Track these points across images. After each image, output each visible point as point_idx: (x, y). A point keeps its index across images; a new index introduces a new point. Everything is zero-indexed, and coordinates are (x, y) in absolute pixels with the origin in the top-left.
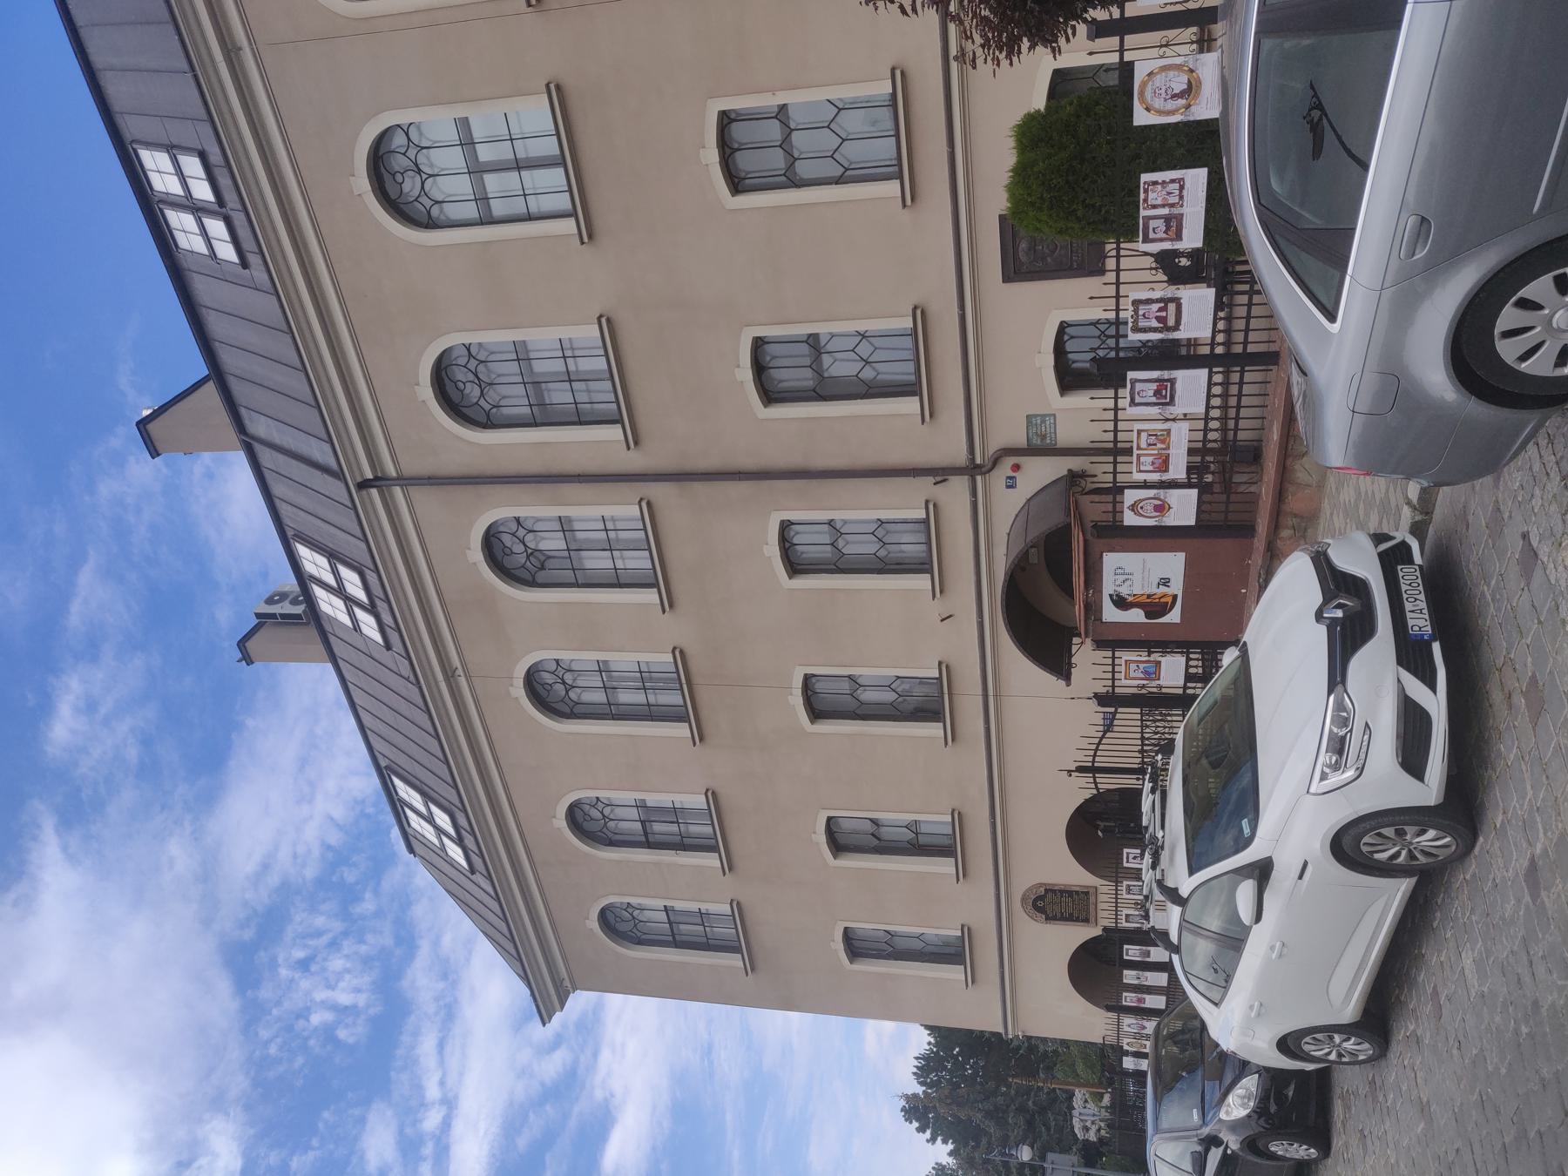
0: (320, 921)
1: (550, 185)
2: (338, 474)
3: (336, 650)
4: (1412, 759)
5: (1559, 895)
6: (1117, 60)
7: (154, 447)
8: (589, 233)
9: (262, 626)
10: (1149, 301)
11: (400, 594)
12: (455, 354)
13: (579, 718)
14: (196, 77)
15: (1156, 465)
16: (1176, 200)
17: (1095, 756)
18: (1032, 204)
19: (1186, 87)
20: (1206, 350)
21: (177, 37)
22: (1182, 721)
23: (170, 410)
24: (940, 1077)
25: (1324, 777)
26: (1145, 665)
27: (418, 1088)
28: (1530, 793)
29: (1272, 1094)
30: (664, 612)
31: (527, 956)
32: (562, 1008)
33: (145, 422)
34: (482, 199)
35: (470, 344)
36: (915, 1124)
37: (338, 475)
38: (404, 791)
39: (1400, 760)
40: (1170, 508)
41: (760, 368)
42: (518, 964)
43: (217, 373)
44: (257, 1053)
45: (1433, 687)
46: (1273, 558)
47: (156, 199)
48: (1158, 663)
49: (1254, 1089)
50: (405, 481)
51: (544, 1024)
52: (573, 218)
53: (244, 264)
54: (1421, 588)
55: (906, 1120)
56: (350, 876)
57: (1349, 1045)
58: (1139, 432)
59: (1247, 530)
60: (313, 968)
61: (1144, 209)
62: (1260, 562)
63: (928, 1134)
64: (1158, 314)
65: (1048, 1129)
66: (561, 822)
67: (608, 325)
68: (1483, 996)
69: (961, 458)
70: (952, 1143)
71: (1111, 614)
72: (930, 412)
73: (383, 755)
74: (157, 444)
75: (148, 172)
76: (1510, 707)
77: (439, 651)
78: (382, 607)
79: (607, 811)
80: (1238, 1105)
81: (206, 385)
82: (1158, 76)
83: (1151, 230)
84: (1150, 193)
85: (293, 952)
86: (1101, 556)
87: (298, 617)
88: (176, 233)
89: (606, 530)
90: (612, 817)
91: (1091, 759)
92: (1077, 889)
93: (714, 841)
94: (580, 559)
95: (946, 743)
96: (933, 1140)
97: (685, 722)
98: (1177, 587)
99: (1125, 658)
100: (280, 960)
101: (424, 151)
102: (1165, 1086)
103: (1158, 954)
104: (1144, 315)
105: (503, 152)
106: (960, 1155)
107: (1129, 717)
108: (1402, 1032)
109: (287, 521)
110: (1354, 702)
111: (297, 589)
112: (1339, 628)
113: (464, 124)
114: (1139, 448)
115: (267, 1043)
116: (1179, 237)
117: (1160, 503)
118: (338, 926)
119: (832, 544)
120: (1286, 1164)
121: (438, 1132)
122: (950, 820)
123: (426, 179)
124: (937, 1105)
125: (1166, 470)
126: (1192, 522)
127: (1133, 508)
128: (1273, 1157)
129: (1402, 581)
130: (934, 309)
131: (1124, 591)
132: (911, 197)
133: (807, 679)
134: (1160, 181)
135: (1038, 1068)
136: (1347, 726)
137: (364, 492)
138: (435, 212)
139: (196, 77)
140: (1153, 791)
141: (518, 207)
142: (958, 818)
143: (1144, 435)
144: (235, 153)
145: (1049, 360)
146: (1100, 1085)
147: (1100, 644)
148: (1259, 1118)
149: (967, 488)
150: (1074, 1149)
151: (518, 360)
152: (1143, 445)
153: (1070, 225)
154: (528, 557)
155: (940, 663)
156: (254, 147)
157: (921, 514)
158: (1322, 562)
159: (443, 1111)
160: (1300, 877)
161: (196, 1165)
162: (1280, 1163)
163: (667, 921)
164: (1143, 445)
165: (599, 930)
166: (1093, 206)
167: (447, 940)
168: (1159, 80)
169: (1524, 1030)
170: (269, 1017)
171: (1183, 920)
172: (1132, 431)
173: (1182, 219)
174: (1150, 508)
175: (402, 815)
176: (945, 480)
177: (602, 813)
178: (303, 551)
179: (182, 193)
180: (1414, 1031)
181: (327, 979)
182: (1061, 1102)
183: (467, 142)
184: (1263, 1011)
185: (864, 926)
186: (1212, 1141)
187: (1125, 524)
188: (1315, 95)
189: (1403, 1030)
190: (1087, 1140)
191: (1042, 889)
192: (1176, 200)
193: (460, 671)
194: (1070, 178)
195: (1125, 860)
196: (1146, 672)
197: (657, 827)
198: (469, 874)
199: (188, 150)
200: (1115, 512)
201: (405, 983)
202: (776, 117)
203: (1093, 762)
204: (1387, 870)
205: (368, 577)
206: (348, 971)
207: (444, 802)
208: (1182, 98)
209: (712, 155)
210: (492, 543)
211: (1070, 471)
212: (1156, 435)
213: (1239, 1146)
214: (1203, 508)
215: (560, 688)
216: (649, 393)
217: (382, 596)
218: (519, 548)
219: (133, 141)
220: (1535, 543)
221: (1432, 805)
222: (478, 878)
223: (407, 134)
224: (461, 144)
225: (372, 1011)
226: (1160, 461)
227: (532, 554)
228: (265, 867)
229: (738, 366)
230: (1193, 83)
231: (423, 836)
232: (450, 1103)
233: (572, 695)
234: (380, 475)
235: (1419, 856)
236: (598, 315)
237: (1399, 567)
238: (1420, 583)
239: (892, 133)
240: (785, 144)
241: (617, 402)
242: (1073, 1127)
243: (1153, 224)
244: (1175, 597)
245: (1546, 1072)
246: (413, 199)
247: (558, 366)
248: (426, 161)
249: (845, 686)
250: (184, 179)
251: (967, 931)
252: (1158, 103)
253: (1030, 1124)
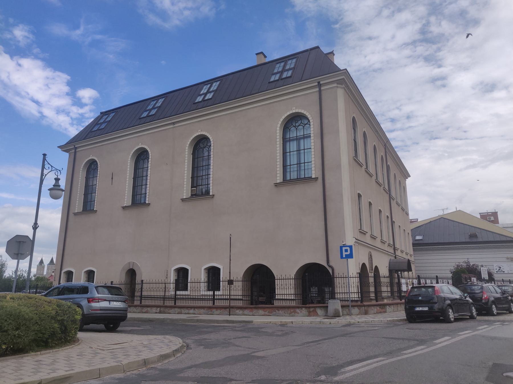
50: (320, 91)
89: (304, 149)
123: (308, 124)
203: (373, 277)
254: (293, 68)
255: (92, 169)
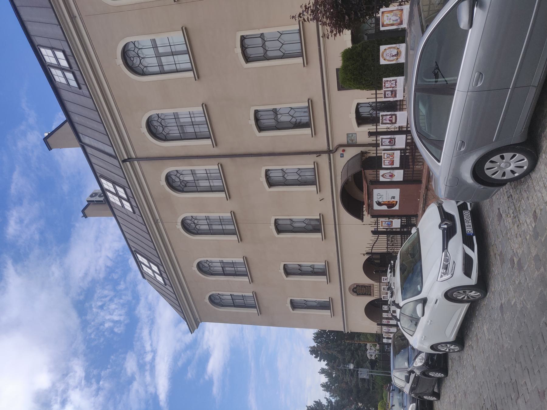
0: (106, 292)
1: (184, 60)
2: (115, 157)
3: (115, 212)
4: (467, 272)
5: (508, 317)
6: (375, 143)
7: (50, 147)
8: (198, 76)
9: (89, 205)
10: (386, 115)
11: (137, 193)
12: (153, 117)
13: (200, 234)
14: (61, 28)
15: (390, 163)
16: (394, 86)
17: (372, 249)
18: (348, 79)
19: (396, 53)
20: (405, 129)
21: (54, 14)
22: (400, 248)
23: (54, 133)
24: (322, 340)
25: (441, 276)
26: (388, 222)
27: (143, 347)
28: (501, 285)
29: (430, 358)
30: (227, 200)
31: (182, 305)
32: (197, 328)
33: (46, 138)
34: (161, 65)
35: (158, 114)
36: (314, 356)
37: (115, 157)
38: (141, 258)
39: (464, 272)
40: (394, 176)
41: (257, 120)
42: (182, 314)
43: (69, 119)
44: (87, 337)
45: (473, 250)
46: (426, 205)
47: (47, 64)
48: (392, 222)
49: (424, 357)
50: (138, 159)
51: (192, 334)
52: (192, 72)
53: (80, 88)
54: (470, 218)
55: (311, 354)
56: (115, 276)
57: (452, 347)
58: (384, 154)
59: (419, 182)
60: (105, 308)
61: (384, 88)
62: (423, 192)
63: (318, 358)
64: (389, 119)
65: (359, 356)
66: (195, 268)
67: (206, 107)
68: (489, 340)
69: (325, 148)
70: (326, 361)
71: (376, 207)
72: (315, 133)
73: (133, 246)
74: (51, 146)
75: (44, 56)
76: (495, 258)
77: (150, 211)
78: (132, 200)
79: (210, 264)
80: (419, 362)
81: (66, 123)
82: (388, 50)
83: (387, 95)
84: (386, 84)
85: (97, 303)
86: (373, 190)
87: (101, 201)
88: (45, 57)
89: (207, 173)
90: (212, 266)
91: (371, 250)
92: (367, 285)
93: (246, 273)
94: (198, 183)
95: (323, 240)
96: (320, 360)
97: (236, 235)
98: (397, 199)
99: (381, 220)
100: (93, 306)
101: (141, 50)
102: (396, 353)
103: (393, 322)
104: (385, 119)
105: (168, 49)
106: (329, 365)
107: (383, 238)
108: (468, 344)
109: (97, 171)
110: (451, 255)
111: (101, 191)
112: (446, 231)
113: (154, 41)
114: (384, 158)
115: (90, 334)
116: (395, 96)
117: (391, 174)
118: (112, 294)
119: (283, 176)
120: (434, 378)
121: (151, 362)
122: (325, 264)
124: (321, 350)
125: (393, 165)
126: (402, 180)
127: (383, 176)
128: (431, 377)
129: (464, 216)
130: (315, 100)
131: (380, 200)
132: (306, 63)
133: (276, 220)
134: (389, 80)
135: (355, 336)
136: (448, 262)
137: (124, 163)
138: (145, 69)
139: (61, 28)
140: (391, 272)
141: (173, 67)
142: (327, 263)
143: (386, 155)
144: (75, 51)
145: (354, 115)
146: (376, 341)
147: (373, 216)
148: (426, 366)
149: (327, 158)
150: (367, 362)
151: (175, 118)
152: (386, 157)
153: (360, 86)
154: (181, 183)
155: (320, 214)
156: (83, 53)
157: (313, 167)
158: (441, 208)
159: (152, 354)
160: (436, 303)
161: (69, 375)
162: (433, 378)
163: (231, 299)
164: (386, 157)
165: (209, 302)
166: (368, 80)
167: (150, 297)
168: (388, 51)
169: (500, 352)
170: (90, 325)
171: (401, 313)
172: (382, 153)
173: (396, 91)
174: (388, 176)
175: (140, 266)
176: (320, 155)
177: (209, 265)
178: (103, 181)
179: (57, 63)
180: (471, 344)
181: (109, 312)
182: (363, 347)
183: (155, 46)
184: (426, 338)
185: (297, 299)
186: (412, 372)
187: (380, 181)
188: (437, 65)
189: (468, 343)
190: (372, 359)
191: (356, 285)
192: (394, 86)
193: (159, 221)
194: (360, 71)
195: (382, 280)
196: (388, 224)
197: (227, 269)
198: (164, 286)
199: (59, 50)
200: (377, 177)
201: (136, 312)
202: (260, 37)
203: (372, 251)
204: (461, 301)
205: (127, 190)
206: (117, 309)
207: (155, 263)
208: (395, 56)
209: (239, 50)
210: (168, 178)
211: (361, 151)
212: (390, 154)
213: (420, 373)
214: (405, 175)
215: (193, 225)
216: (220, 129)
217: (132, 197)
218: (177, 180)
219: (38, 45)
220: (501, 212)
221: (474, 284)
222: (167, 287)
223: (134, 44)
224: (153, 47)
225: (126, 322)
226: (391, 162)
227: (182, 181)
228: (86, 274)
229: (250, 119)
230: (398, 52)
231: (148, 273)
232: (154, 352)
233: (197, 227)
234: (129, 157)
235: (470, 297)
236: (202, 103)
237: (464, 211)
238: (469, 214)
239: (299, 41)
240: (263, 46)
241: (209, 131)
242: (367, 355)
243: (387, 93)
244: (397, 202)
245: (506, 366)
246: (138, 65)
247: (189, 120)
248: (141, 52)
249: (289, 222)
250: (57, 59)
251: (331, 299)
252: (388, 58)
253: (352, 354)
254: (61, 71)
255: (221, 302)
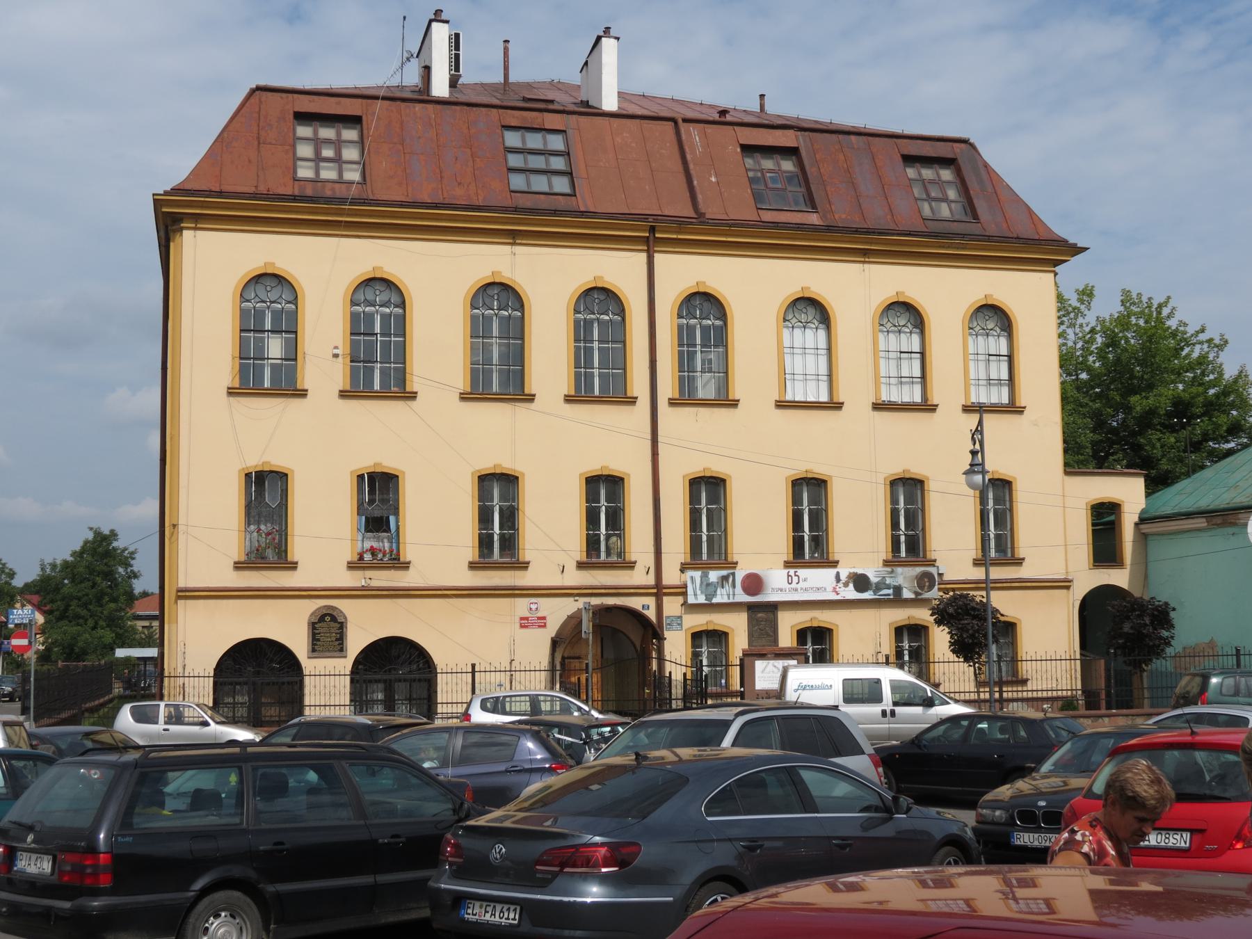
191: (343, 620)
